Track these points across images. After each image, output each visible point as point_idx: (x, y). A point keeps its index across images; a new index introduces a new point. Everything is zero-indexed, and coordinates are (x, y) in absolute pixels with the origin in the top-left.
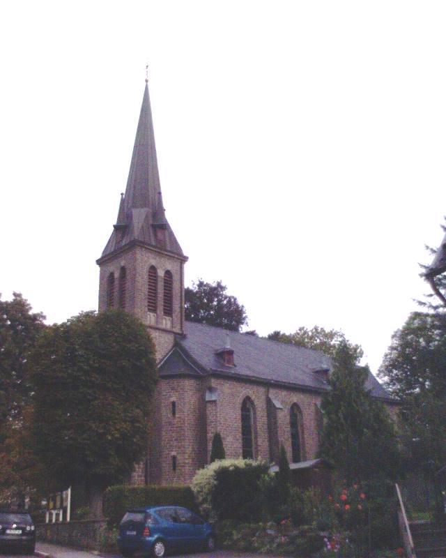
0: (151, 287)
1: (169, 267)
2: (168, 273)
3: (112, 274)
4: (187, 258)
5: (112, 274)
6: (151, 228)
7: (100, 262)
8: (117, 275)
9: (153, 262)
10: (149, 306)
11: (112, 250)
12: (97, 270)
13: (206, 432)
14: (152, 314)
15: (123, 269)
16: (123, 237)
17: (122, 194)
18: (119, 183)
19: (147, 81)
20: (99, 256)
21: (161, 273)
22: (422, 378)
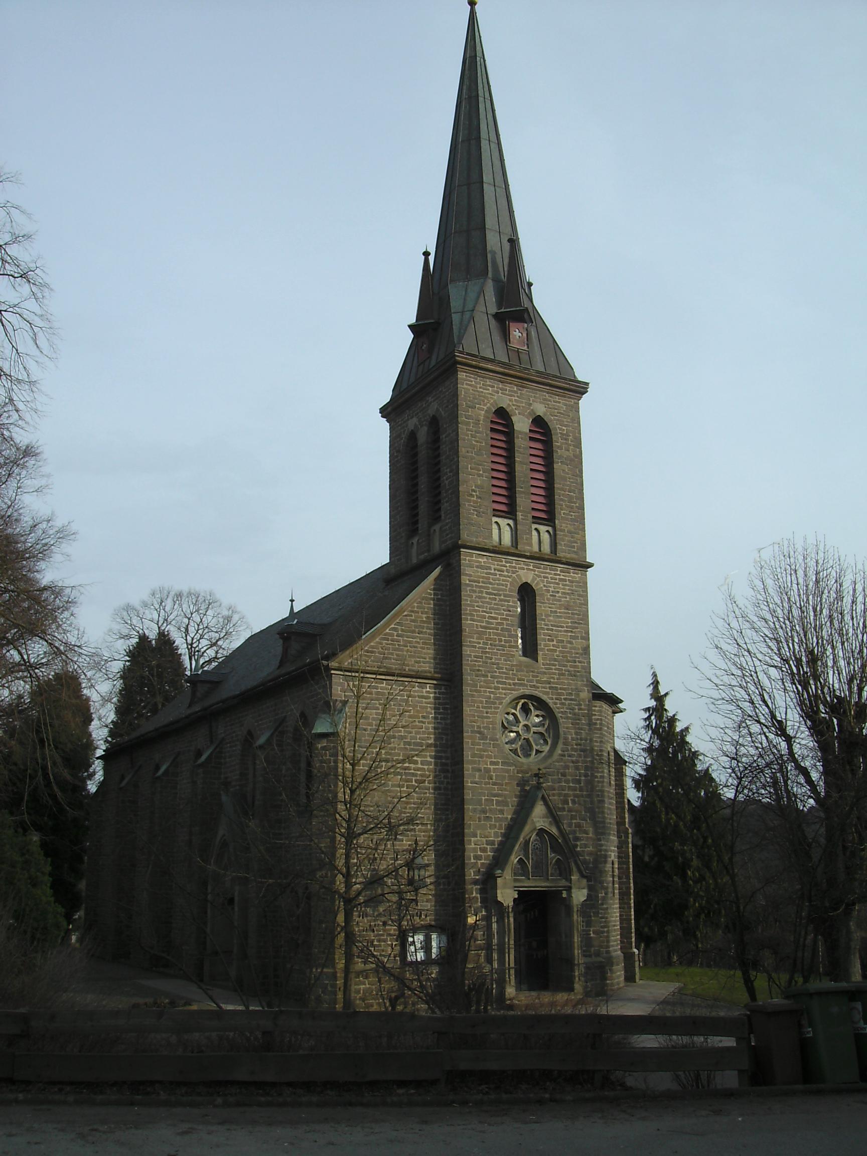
0: (496, 474)
1: (540, 409)
2: (539, 422)
3: (413, 436)
4: (587, 384)
5: (413, 436)
6: (493, 322)
7: (386, 412)
8: (423, 436)
9: (505, 402)
10: (531, 439)
11: (412, 380)
12: (383, 427)
13: (462, 867)
14: (503, 522)
15: (434, 422)
16: (430, 351)
17: (426, 254)
18: (418, 229)
19: (292, 601)
20: (386, 397)
21: (522, 425)
22: (713, 840)
